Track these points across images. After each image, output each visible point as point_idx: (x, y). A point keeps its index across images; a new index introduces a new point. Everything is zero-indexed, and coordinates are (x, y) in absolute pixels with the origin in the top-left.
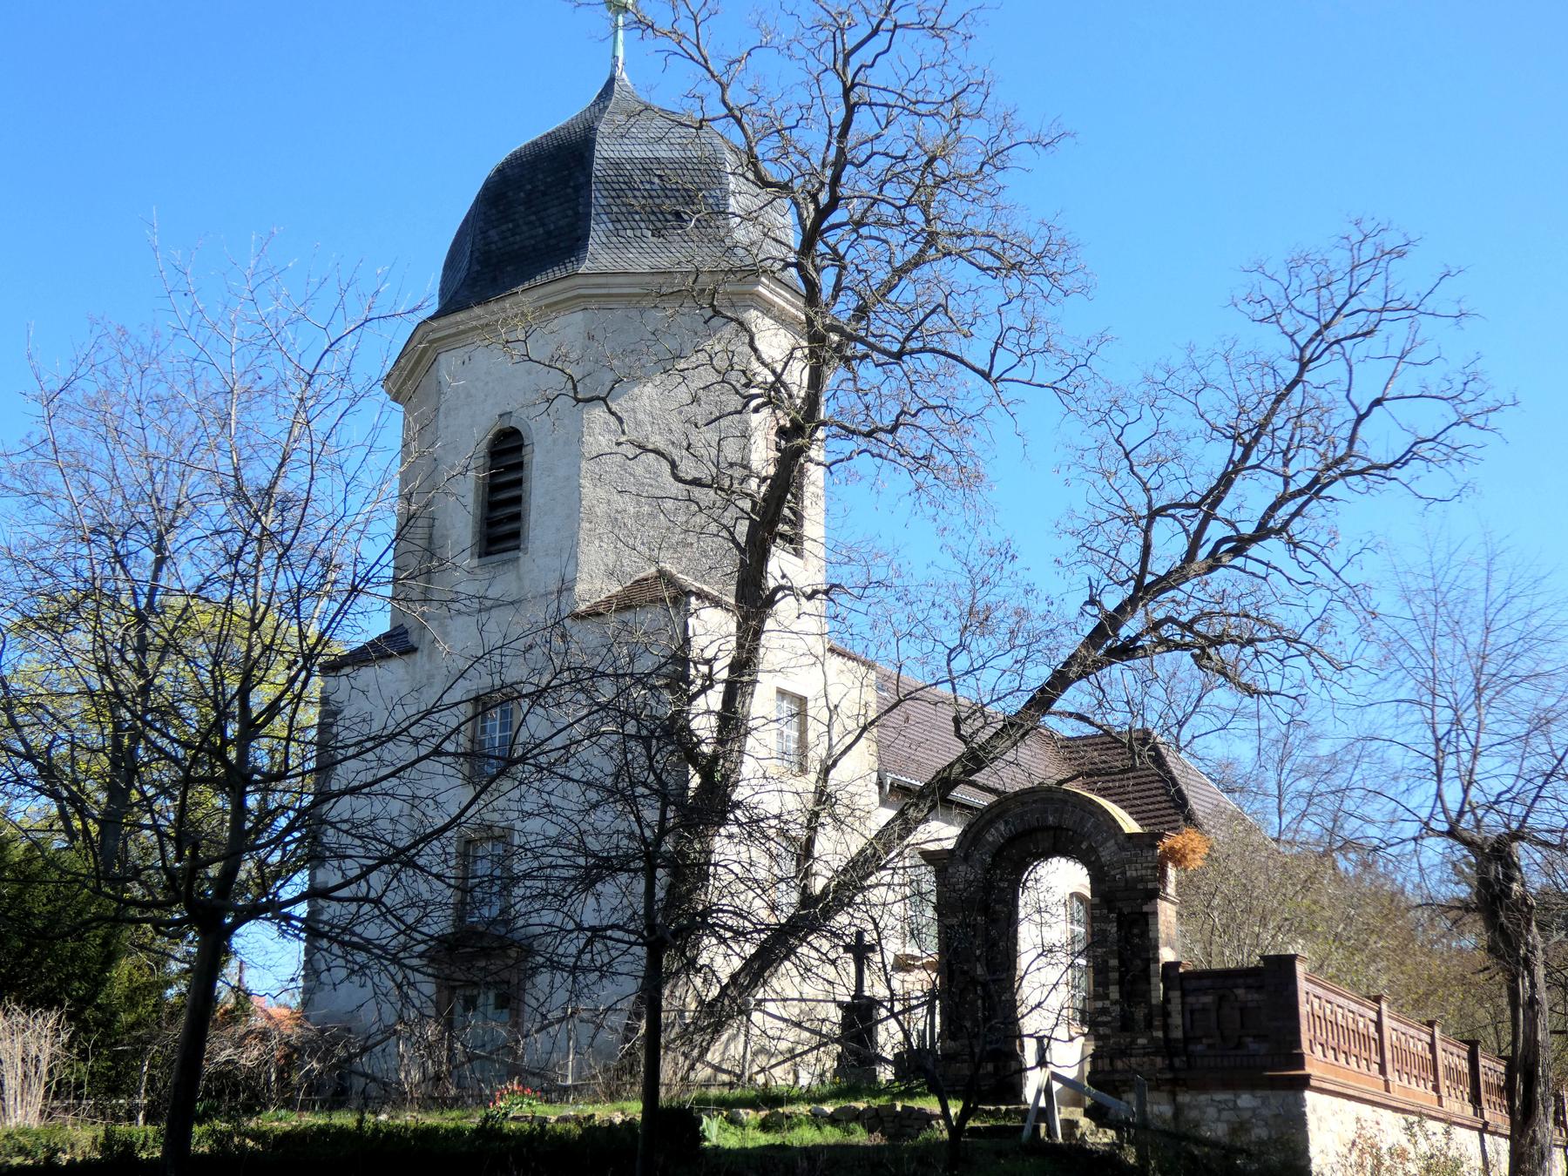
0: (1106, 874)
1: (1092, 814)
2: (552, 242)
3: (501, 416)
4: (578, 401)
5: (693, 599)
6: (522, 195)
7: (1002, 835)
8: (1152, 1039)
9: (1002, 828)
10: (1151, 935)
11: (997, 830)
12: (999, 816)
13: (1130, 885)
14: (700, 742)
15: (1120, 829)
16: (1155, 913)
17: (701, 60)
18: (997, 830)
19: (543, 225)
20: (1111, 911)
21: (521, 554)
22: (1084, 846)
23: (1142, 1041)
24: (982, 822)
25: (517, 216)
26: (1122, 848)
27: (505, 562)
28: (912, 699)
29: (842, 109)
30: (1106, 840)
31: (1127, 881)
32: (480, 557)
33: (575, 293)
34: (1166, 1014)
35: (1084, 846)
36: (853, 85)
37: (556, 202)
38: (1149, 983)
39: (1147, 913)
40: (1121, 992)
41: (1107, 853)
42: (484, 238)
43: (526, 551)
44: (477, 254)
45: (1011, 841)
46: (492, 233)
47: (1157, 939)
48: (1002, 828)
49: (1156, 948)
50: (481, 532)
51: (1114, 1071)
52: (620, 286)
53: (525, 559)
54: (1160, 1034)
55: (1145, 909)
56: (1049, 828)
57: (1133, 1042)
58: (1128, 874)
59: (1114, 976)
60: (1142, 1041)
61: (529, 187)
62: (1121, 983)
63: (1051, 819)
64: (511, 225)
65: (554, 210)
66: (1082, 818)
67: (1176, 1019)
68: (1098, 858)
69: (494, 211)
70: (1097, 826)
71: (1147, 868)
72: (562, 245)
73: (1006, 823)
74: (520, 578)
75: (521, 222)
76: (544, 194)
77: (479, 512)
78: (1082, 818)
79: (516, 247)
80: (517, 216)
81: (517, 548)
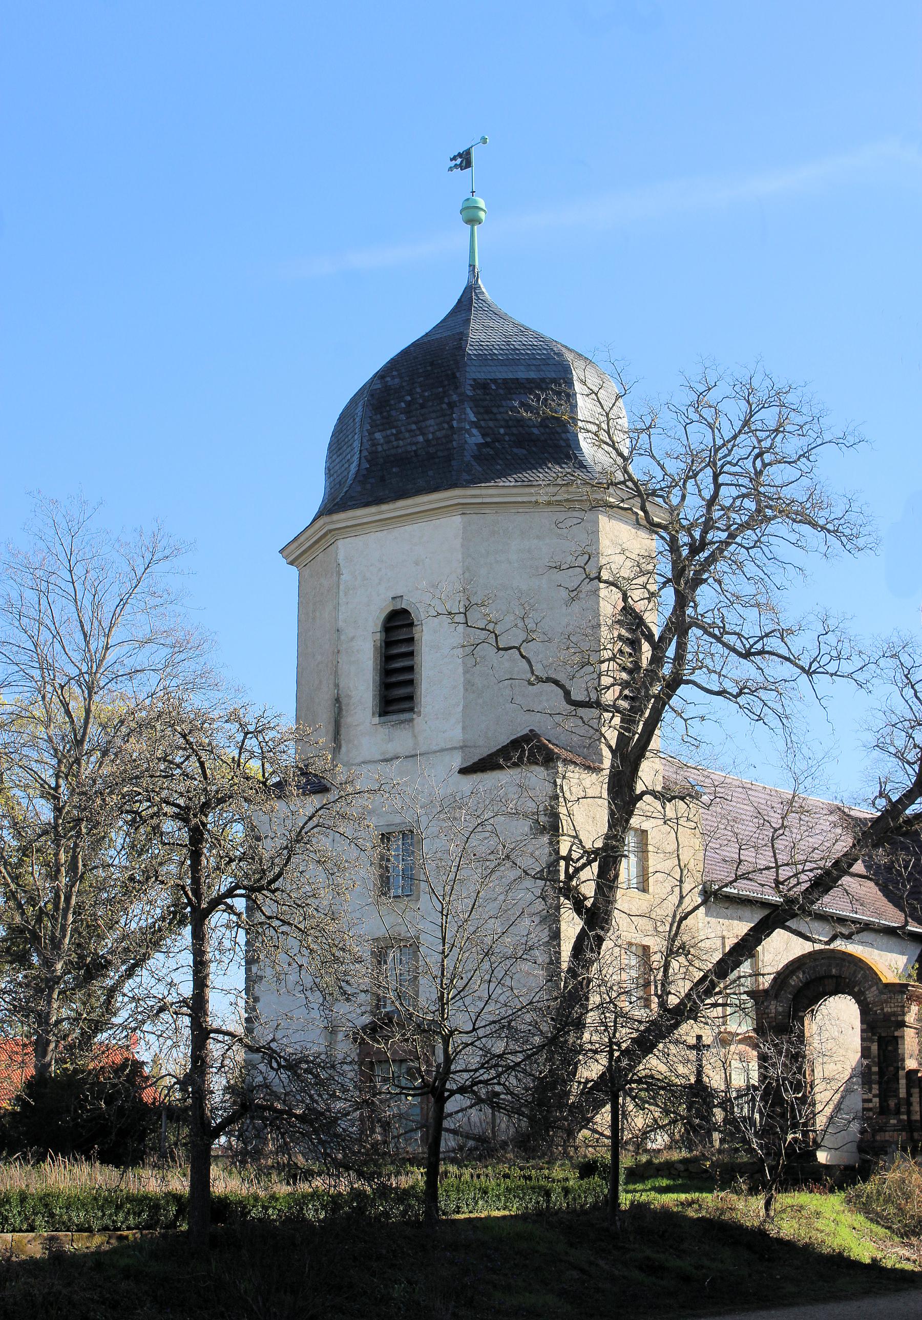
0: (871, 1010)
1: (862, 969)
2: (432, 450)
3: (393, 598)
4: (499, 649)
5: (560, 764)
6: (403, 405)
7: (801, 981)
8: (900, 1121)
9: (801, 976)
10: (900, 1051)
11: (798, 977)
12: (799, 968)
13: (887, 1017)
14: (586, 898)
15: (880, 980)
16: (903, 1037)
17: (610, 443)
18: (798, 977)
19: (423, 434)
20: (874, 1034)
21: (415, 716)
22: (856, 990)
23: (893, 1121)
24: (787, 972)
25: (399, 423)
26: (881, 993)
27: (402, 722)
28: (744, 878)
29: (712, 486)
30: (871, 987)
31: (884, 1014)
32: (380, 716)
33: (456, 501)
34: (909, 1104)
35: (856, 990)
36: (721, 473)
37: (433, 415)
38: (898, 1083)
39: (897, 1037)
40: (880, 1090)
41: (871, 995)
42: (371, 440)
43: (419, 714)
44: (365, 453)
45: (807, 985)
46: (378, 435)
47: (903, 1054)
48: (801, 976)
49: (903, 1060)
50: (380, 695)
51: (875, 1141)
52: (491, 496)
53: (418, 721)
54: (905, 1117)
55: (896, 1034)
56: (832, 977)
57: (888, 1122)
58: (885, 1010)
59: (875, 1077)
60: (893, 1121)
61: (408, 398)
62: (880, 1083)
63: (834, 970)
64: (394, 431)
65: (431, 422)
66: (855, 972)
67: (916, 1107)
68: (865, 999)
69: (379, 416)
70: (865, 977)
71: (898, 1006)
72: (440, 454)
73: (804, 973)
74: (415, 736)
75: (403, 429)
76: (422, 406)
77: (378, 679)
78: (855, 972)
79: (400, 451)
80: (399, 423)
81: (411, 710)
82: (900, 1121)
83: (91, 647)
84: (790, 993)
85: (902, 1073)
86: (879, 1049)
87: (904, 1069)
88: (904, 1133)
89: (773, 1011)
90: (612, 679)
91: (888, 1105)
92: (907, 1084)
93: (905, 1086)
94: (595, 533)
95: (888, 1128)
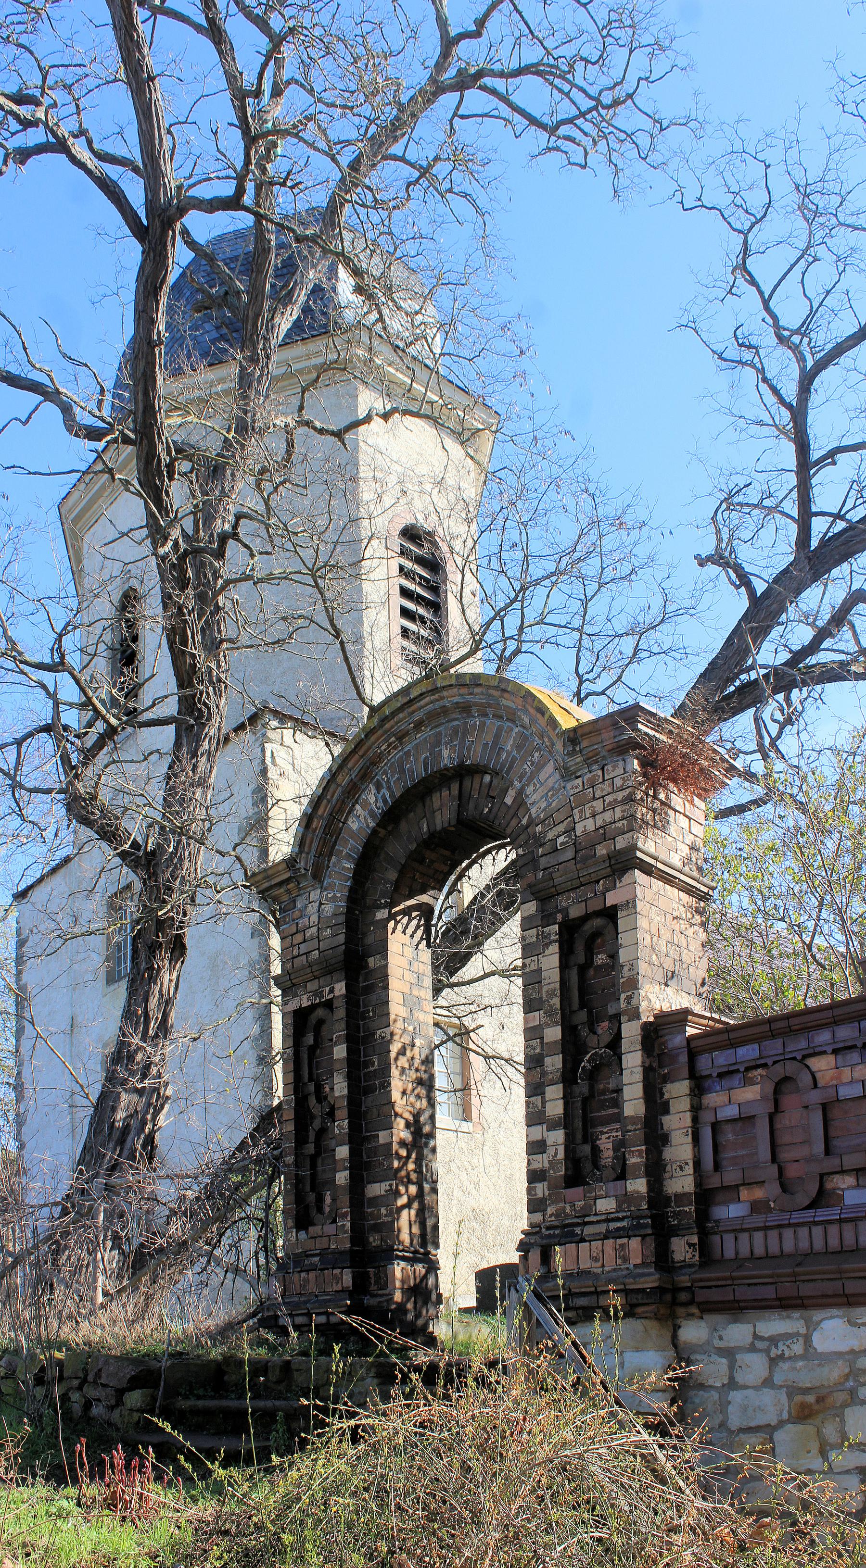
8: (625, 1199)
16: (630, 904)
49: (633, 984)
55: (611, 899)
60: (606, 1205)
63: (446, 753)
66: (497, 736)
71: (612, 806)
78: (497, 736)
82: (625, 1199)
83: (530, 81)
84: (348, 856)
85: (631, 1031)
86: (564, 966)
87: (635, 1014)
88: (635, 1243)
89: (314, 918)
90: (577, 616)
91: (596, 1151)
92: (648, 1071)
93: (638, 1075)
94: (338, 1059)
95: (588, 1230)
